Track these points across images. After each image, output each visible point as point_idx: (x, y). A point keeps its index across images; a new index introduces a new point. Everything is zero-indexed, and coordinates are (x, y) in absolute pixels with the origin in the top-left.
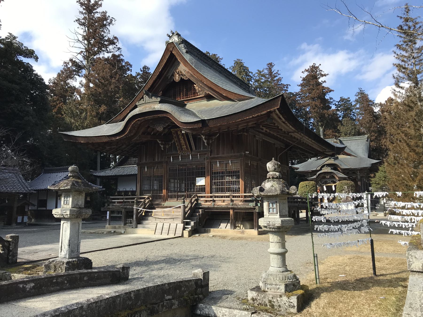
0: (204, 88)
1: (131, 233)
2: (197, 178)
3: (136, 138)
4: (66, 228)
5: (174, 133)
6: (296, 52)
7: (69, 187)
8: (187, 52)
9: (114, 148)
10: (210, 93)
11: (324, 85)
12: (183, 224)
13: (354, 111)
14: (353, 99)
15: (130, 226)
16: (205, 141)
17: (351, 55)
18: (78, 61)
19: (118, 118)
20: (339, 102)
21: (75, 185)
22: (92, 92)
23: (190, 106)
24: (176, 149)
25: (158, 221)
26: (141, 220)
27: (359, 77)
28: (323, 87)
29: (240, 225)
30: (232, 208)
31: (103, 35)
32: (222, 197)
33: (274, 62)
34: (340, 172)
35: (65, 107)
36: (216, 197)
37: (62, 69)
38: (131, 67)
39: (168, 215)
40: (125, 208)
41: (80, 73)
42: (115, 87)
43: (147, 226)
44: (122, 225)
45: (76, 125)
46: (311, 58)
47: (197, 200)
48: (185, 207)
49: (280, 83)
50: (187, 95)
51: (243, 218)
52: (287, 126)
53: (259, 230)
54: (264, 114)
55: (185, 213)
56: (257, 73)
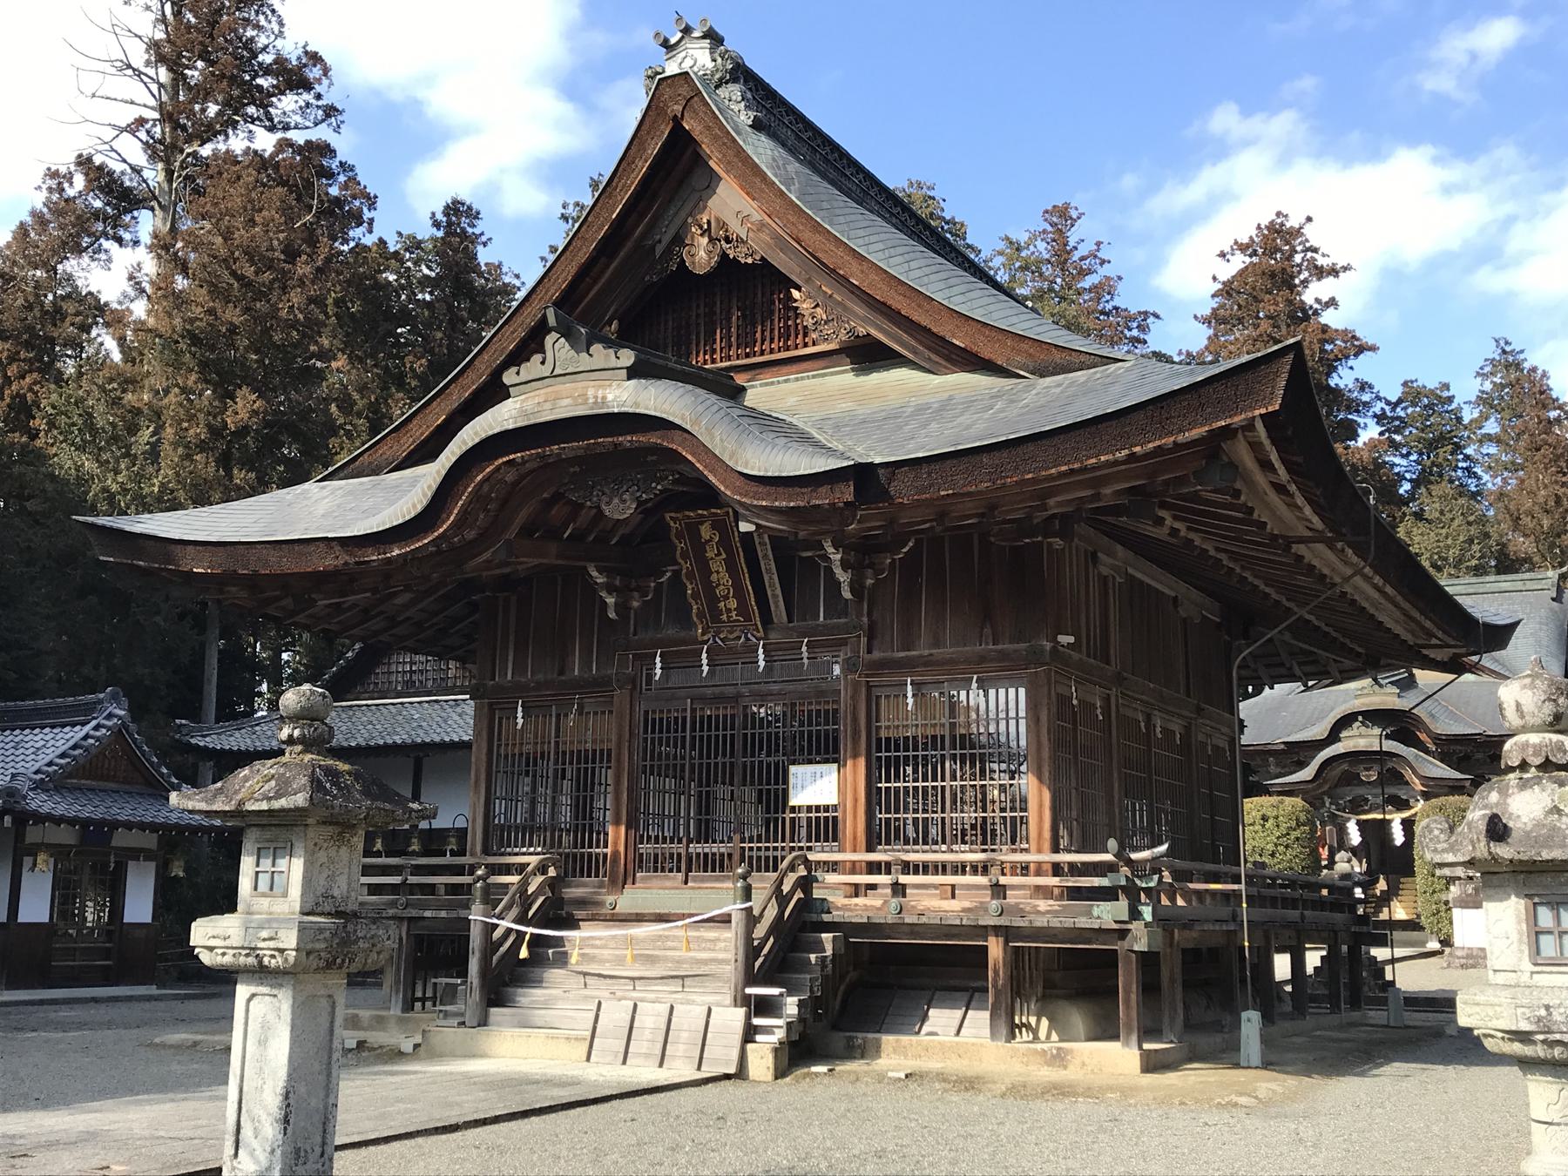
0: (845, 308)
1: (454, 1055)
2: (793, 769)
3: (486, 555)
4: (266, 1027)
5: (680, 536)
6: (1187, 153)
7: (300, 800)
8: (757, 126)
9: (355, 605)
10: (873, 332)
11: (1329, 318)
12: (742, 1011)
13: (1469, 451)
14: (1466, 390)
15: (446, 1015)
16: (843, 577)
17: (1456, 172)
18: (117, 167)
19: (383, 449)
20: (1395, 405)
21: (327, 792)
22: (192, 321)
23: (761, 393)
24: (683, 617)
25: (599, 989)
26: (506, 980)
27: (1489, 281)
28: (1325, 329)
29: (1033, 1020)
30: (997, 930)
31: (252, 39)
32: (942, 868)
33: (1078, 201)
34: (1427, 752)
35: (50, 398)
36: (907, 867)
37: (39, 206)
38: (372, 206)
39: (651, 960)
40: (410, 919)
41: (126, 227)
42: (311, 300)
43: (540, 1016)
44: (396, 1010)
45: (105, 490)
46: (1253, 181)
47: (806, 884)
48: (751, 919)
49: (1109, 307)
50: (747, 341)
51: (1049, 985)
52: (1293, 506)
53: (1146, 1046)
54: (1194, 443)
55: (752, 952)
56: (1001, 253)
